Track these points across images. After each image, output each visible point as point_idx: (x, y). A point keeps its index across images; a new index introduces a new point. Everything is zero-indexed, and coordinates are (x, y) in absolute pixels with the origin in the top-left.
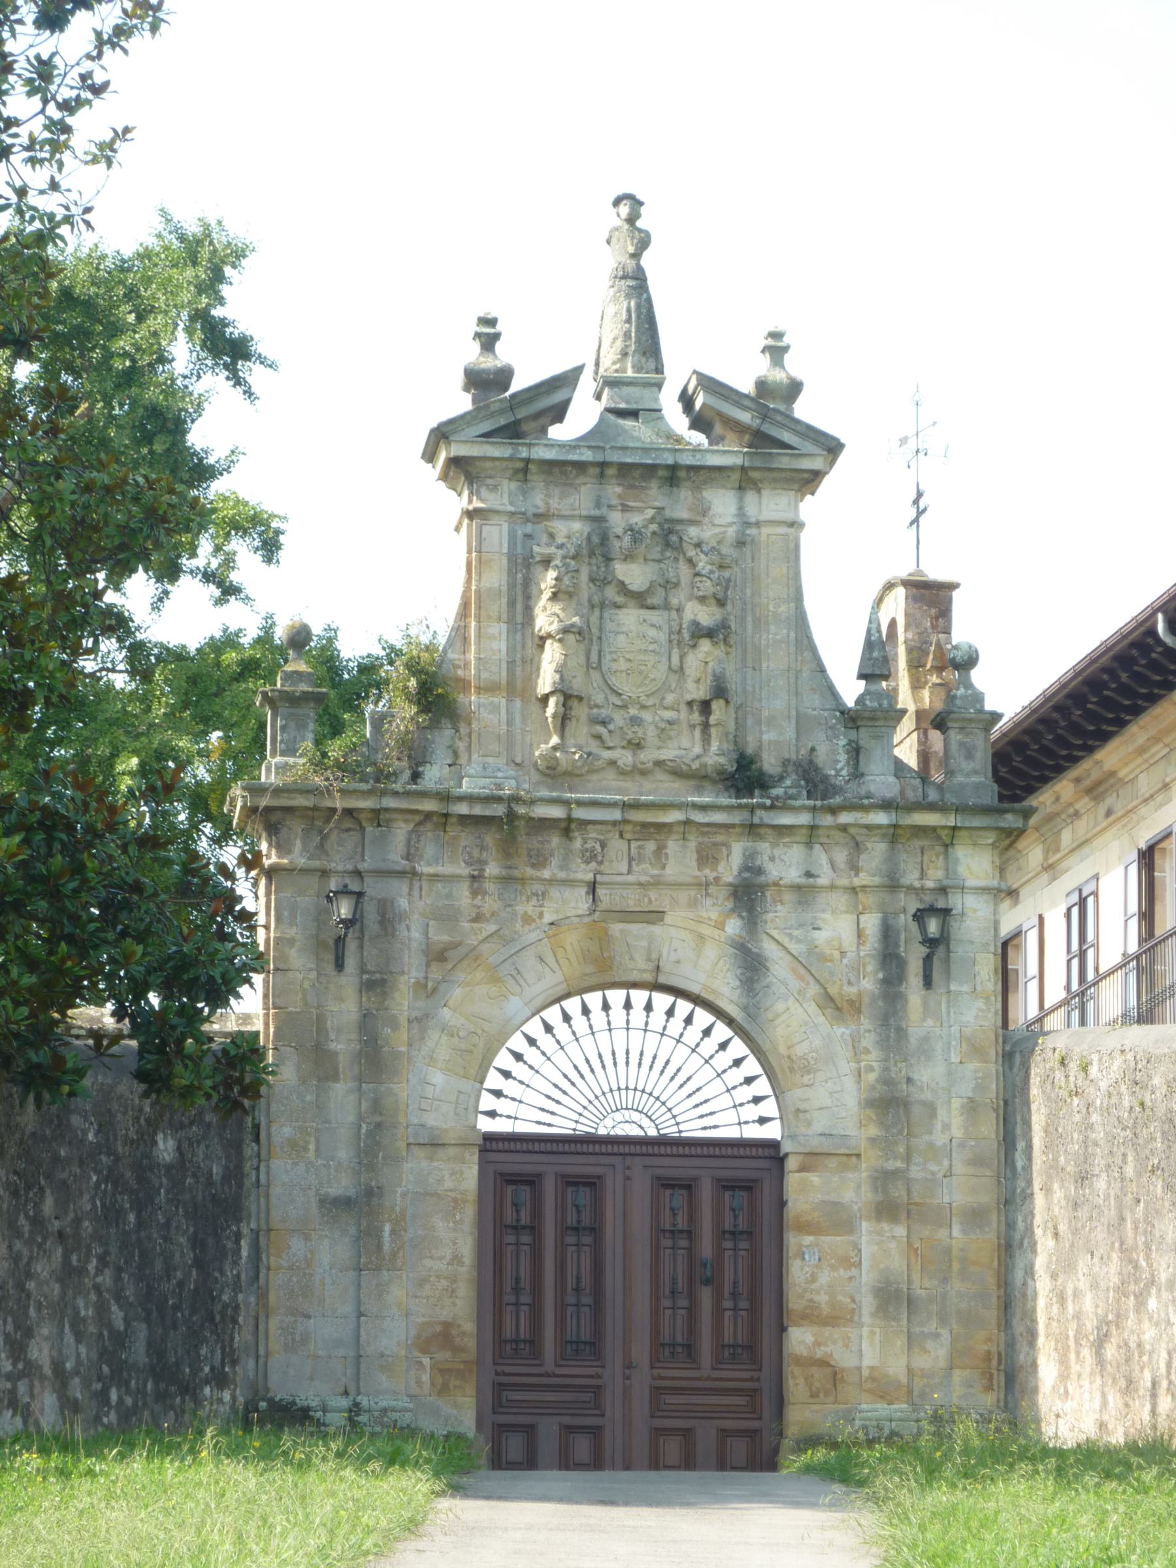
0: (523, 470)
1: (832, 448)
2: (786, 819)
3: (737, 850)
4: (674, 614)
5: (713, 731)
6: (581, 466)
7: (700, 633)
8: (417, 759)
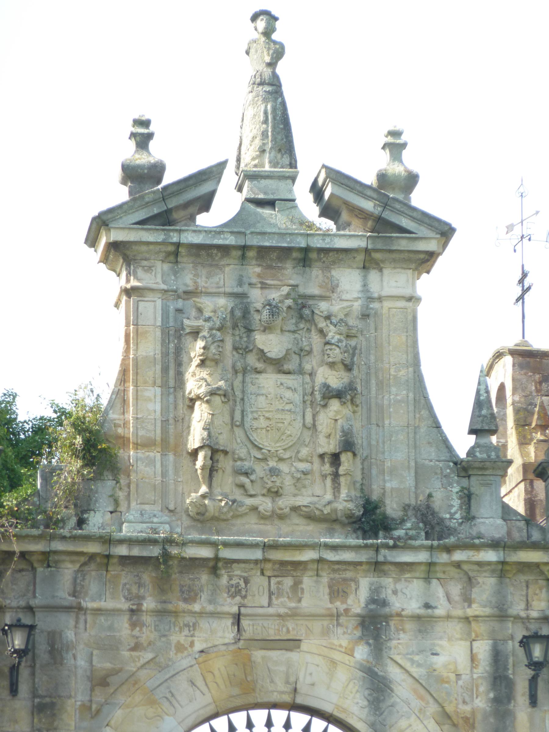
0: (175, 253)
1: (446, 232)
2: (407, 557)
3: (364, 585)
4: (307, 378)
5: (342, 480)
6: (225, 249)
7: (330, 394)
8: (83, 507)
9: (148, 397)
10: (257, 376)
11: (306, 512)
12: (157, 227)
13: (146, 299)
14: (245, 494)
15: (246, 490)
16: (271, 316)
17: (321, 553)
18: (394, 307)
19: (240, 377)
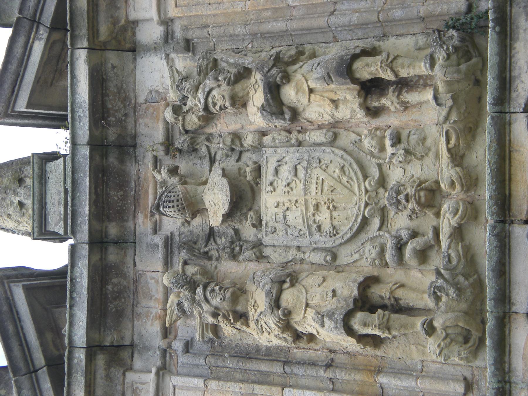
4: (267, 140)
5: (404, 73)
7: (275, 106)
10: (264, 223)
11: (458, 138)
12: (66, 384)
14: (436, 248)
16: (171, 205)
17: (518, 110)
19: (267, 252)
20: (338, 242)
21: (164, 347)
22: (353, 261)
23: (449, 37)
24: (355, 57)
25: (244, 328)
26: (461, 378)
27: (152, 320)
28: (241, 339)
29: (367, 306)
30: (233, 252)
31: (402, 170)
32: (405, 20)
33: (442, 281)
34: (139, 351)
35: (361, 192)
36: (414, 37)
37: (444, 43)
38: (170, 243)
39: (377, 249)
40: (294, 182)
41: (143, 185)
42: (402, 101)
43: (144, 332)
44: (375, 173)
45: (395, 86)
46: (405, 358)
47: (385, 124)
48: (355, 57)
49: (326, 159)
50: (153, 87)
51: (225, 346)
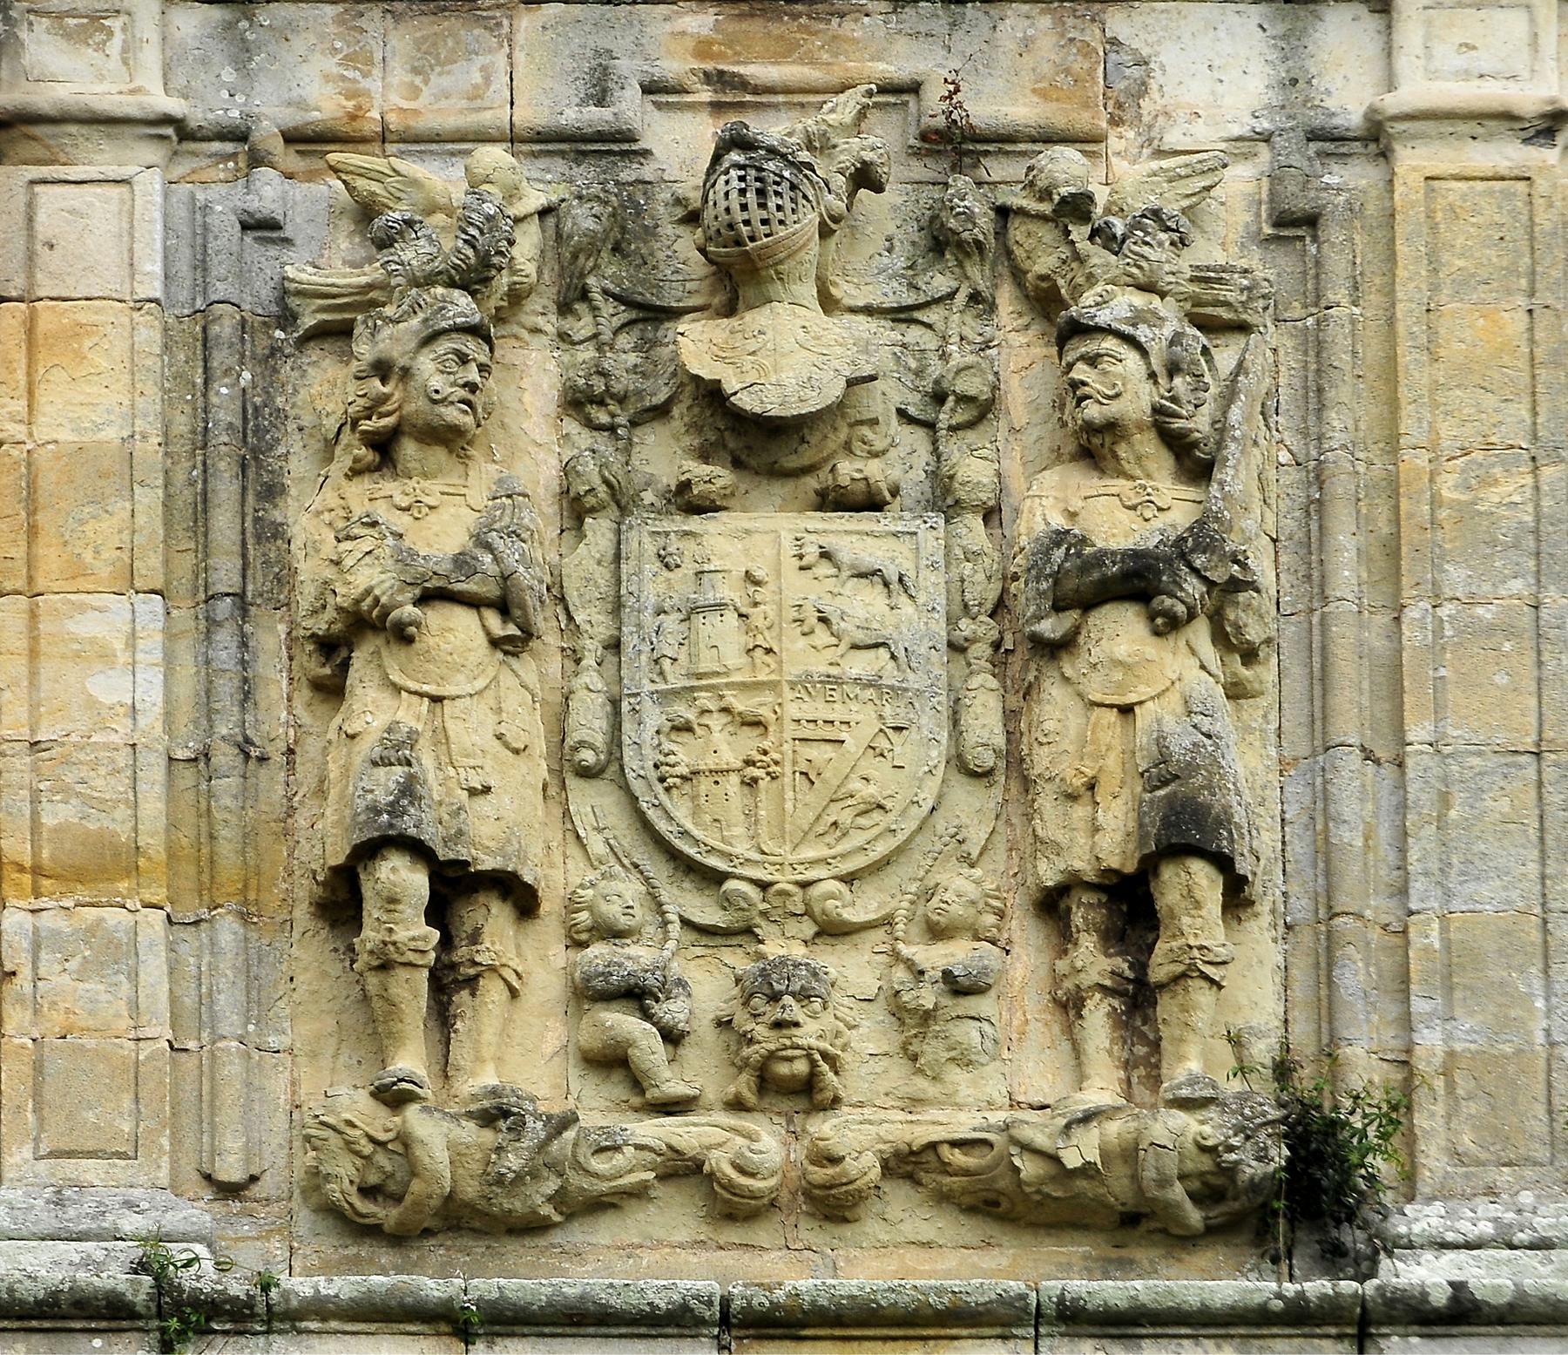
4: (973, 530)
9: (93, 641)
10: (694, 523)
11: (966, 1172)
13: (74, 173)
14: (636, 1101)
15: (637, 1083)
16: (751, 197)
18: (1454, 169)
19: (599, 530)
20: (637, 787)
21: (255, 136)
22: (582, 833)
23: (1266, 1149)
24: (1223, 862)
25: (342, 462)
26: (255, 1171)
27: (343, 78)
28: (301, 429)
29: (444, 890)
30: (591, 402)
31: (871, 992)
32: (1329, 997)
33: (543, 1135)
34: (230, 26)
35: (800, 868)
36: (1277, 1023)
37: (1248, 1138)
38: (615, 147)
39: (623, 919)
40: (834, 641)
41: (815, 33)
42: (1083, 1000)
43: (299, 44)
44: (860, 907)
45: (1129, 974)
46: (295, 995)
47: (1015, 938)
48: (1223, 862)
49: (908, 748)
50: (1157, 74)
51: (275, 371)
